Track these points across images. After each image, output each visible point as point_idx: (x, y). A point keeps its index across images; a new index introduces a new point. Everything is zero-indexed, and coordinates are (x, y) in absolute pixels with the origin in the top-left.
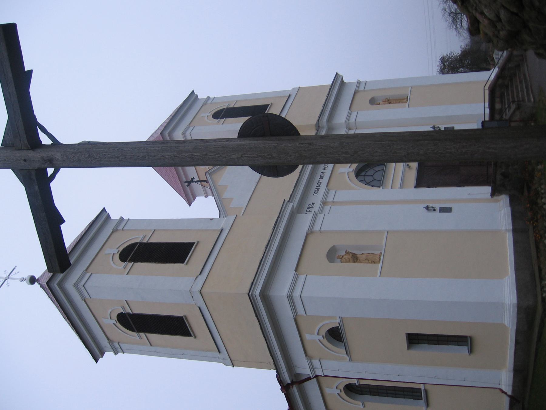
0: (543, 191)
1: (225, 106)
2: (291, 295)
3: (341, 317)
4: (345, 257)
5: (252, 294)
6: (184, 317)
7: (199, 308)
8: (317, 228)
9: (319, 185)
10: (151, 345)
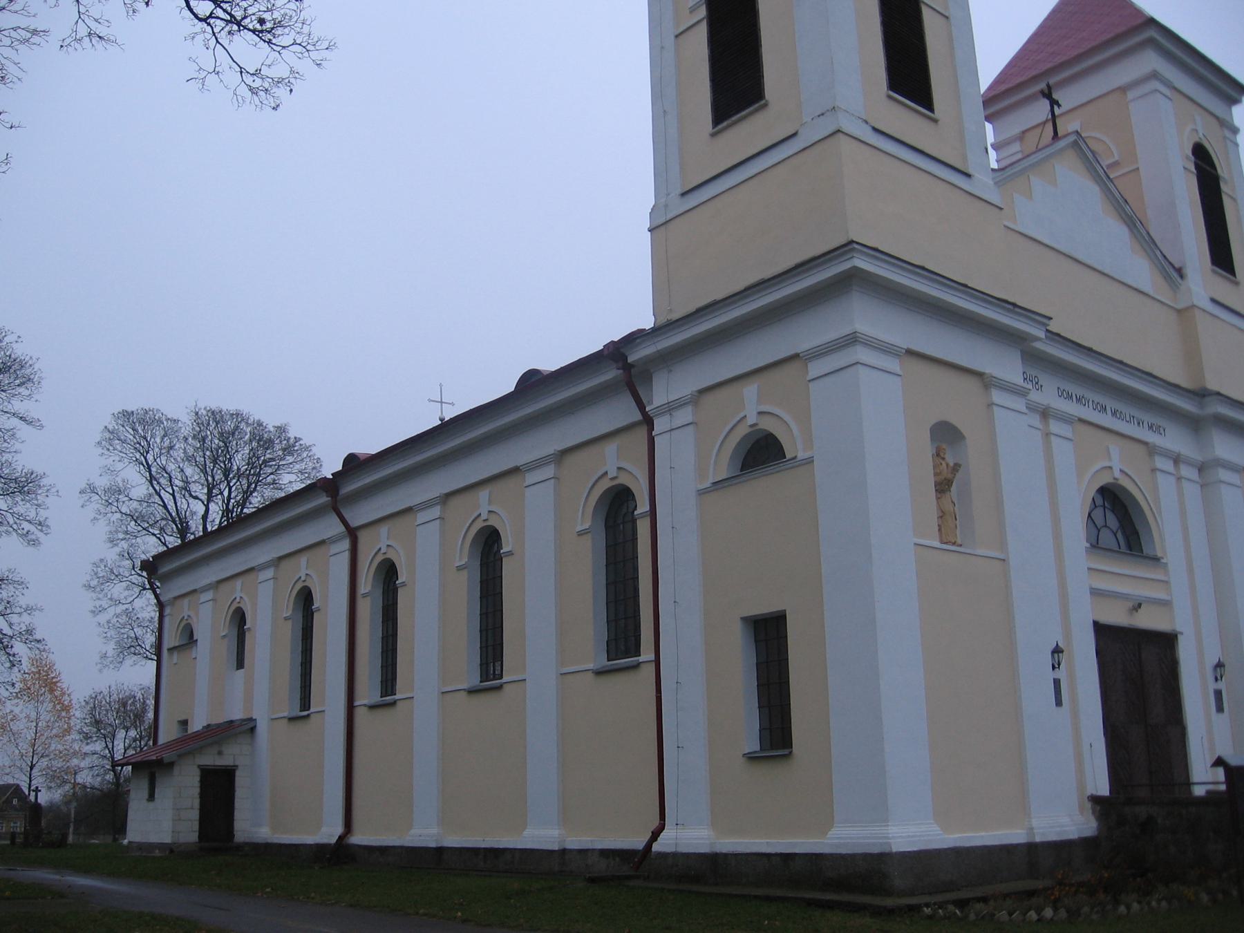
0: (1154, 904)
1: (1222, 171)
2: (860, 342)
3: (813, 461)
4: (944, 464)
5: (854, 249)
6: (763, 102)
7: (795, 135)
8: (997, 396)
9: (1079, 400)
10: (677, 36)
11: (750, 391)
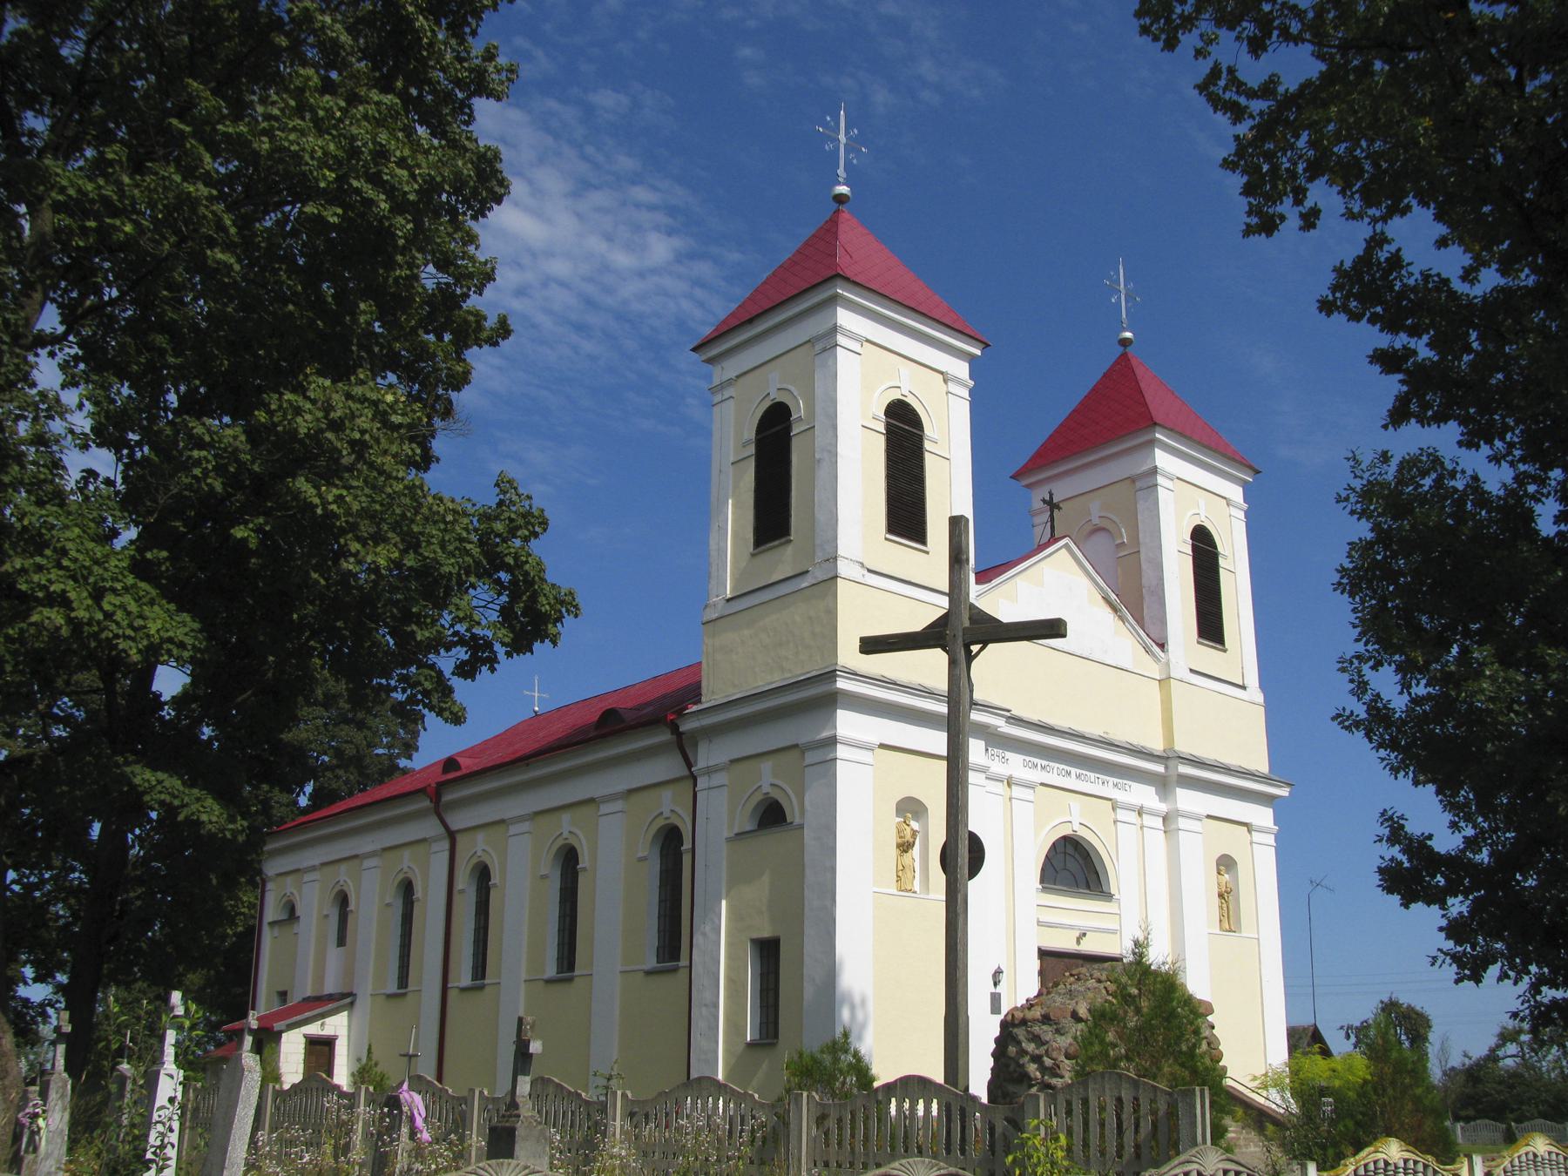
4: (908, 829)
11: (766, 766)
